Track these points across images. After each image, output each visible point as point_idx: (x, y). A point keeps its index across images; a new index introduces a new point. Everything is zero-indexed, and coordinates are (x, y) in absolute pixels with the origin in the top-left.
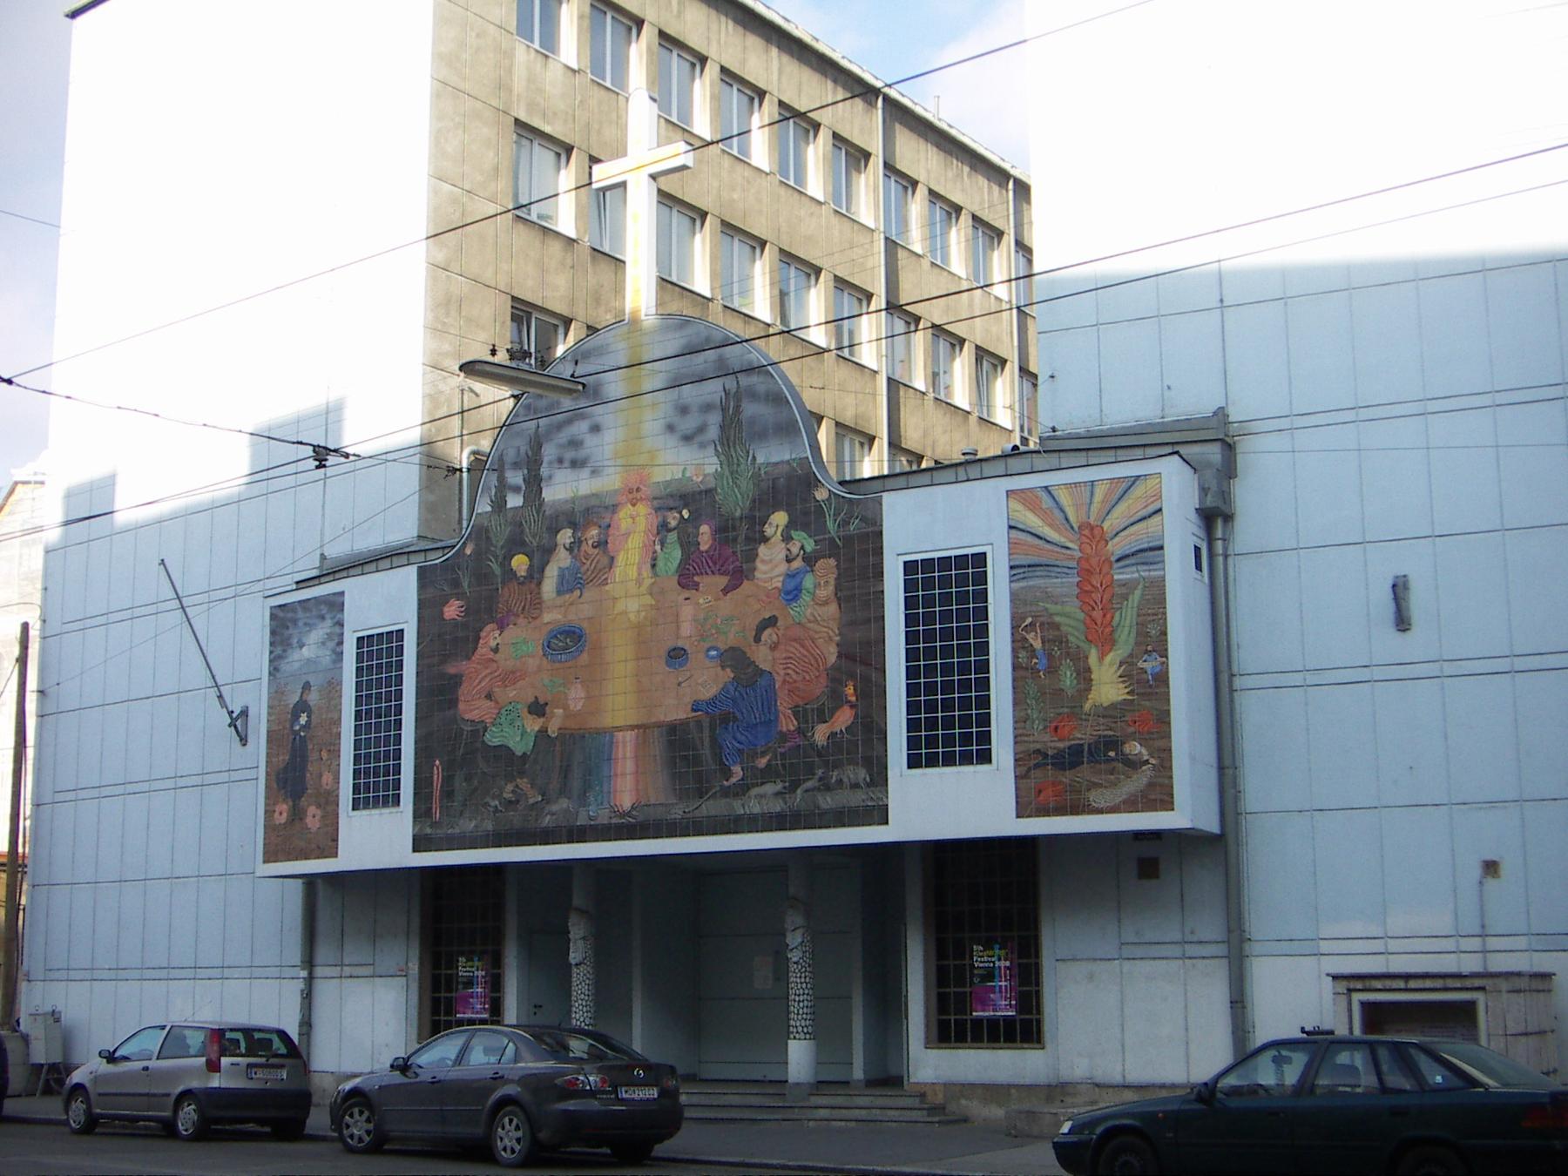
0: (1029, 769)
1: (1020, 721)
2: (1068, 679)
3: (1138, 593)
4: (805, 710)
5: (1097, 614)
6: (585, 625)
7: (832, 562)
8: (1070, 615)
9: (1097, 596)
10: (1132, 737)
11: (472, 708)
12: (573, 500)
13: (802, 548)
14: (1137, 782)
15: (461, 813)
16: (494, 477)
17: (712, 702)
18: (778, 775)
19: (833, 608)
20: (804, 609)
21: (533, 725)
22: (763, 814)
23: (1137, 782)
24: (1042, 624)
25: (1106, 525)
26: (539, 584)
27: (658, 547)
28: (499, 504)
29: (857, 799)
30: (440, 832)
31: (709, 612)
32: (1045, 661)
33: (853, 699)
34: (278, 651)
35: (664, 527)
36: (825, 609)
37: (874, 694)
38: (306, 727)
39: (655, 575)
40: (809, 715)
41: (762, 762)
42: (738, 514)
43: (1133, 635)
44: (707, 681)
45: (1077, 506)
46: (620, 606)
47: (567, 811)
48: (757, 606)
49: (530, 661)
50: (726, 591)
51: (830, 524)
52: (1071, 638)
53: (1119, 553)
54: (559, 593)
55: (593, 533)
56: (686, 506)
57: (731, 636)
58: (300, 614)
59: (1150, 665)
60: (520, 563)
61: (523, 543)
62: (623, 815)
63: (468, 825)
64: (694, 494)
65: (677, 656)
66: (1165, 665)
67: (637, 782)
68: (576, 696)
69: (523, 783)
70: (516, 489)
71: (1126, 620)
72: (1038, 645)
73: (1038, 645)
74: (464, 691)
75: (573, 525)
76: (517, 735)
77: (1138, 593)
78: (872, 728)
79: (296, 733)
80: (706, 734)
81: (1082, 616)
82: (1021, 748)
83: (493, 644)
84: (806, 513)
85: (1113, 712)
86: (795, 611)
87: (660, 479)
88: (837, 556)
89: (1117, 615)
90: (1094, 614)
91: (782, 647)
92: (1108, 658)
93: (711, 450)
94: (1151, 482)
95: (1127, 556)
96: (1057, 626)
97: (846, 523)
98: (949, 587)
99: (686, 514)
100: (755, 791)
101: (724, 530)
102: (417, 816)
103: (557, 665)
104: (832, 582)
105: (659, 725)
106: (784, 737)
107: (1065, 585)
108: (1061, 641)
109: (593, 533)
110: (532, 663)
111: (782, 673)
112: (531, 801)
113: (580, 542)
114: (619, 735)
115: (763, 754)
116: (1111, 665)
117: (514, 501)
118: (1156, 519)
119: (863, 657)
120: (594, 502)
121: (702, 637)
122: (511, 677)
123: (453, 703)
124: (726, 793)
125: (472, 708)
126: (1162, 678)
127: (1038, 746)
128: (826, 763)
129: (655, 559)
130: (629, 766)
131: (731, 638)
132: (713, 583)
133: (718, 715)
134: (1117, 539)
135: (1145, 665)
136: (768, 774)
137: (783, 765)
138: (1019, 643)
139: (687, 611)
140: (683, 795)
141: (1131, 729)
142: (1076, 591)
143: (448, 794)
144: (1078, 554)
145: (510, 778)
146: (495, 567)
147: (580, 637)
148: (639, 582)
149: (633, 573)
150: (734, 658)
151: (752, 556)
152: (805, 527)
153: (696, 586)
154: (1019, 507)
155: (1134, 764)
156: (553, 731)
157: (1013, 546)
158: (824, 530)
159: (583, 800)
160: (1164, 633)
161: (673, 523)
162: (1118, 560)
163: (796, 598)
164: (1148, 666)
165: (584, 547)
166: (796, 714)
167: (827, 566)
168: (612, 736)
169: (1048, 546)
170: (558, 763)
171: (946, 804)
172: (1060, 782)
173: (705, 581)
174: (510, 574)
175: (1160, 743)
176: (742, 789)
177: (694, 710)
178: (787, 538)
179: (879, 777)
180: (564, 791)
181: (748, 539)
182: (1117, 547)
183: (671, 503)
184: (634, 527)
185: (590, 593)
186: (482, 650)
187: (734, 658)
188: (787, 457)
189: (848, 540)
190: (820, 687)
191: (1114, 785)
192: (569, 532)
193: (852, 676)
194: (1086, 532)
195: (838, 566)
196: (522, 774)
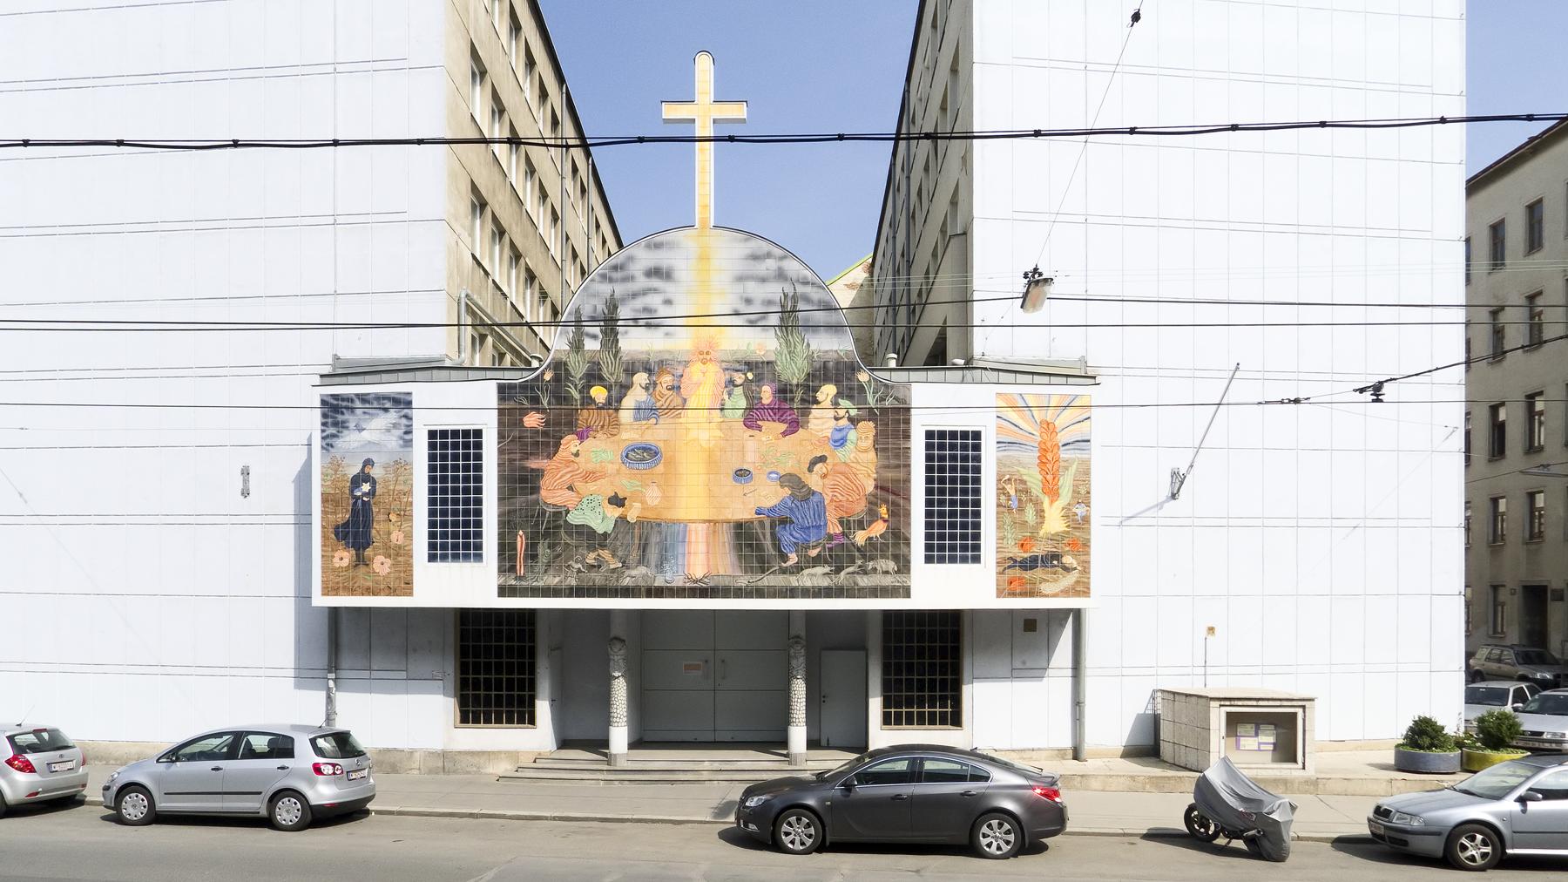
2: (1030, 515)
5: (1049, 477)
6: (661, 445)
7: (871, 424)
8: (1034, 478)
9: (1049, 466)
11: (552, 494)
14: (1071, 579)
17: (771, 510)
18: (826, 562)
19: (872, 454)
20: (846, 454)
21: (614, 513)
23: (1071, 579)
29: (888, 581)
31: (773, 449)
34: (332, 430)
37: (900, 513)
38: (372, 493)
41: (814, 553)
42: (795, 382)
44: (769, 495)
46: (693, 434)
47: (644, 576)
50: (785, 434)
56: (750, 370)
58: (358, 404)
59: (1080, 511)
60: (599, 394)
61: (601, 379)
63: (552, 580)
65: (742, 474)
68: (653, 496)
69: (606, 554)
70: (594, 337)
72: (1012, 493)
73: (1012, 493)
74: (545, 483)
75: (649, 371)
76: (601, 519)
78: (898, 537)
79: (357, 498)
80: (768, 531)
83: (574, 450)
84: (851, 389)
85: (1053, 538)
88: (875, 421)
96: (1024, 482)
99: (750, 376)
100: (806, 572)
101: (783, 391)
106: (831, 537)
107: (1031, 457)
108: (1027, 491)
109: (667, 380)
110: (611, 468)
113: (655, 384)
115: (814, 547)
117: (591, 345)
119: (892, 492)
122: (590, 476)
123: (535, 490)
124: (784, 571)
125: (552, 494)
128: (864, 557)
130: (702, 548)
131: (789, 466)
133: (780, 520)
136: (817, 561)
138: (1001, 491)
143: (532, 556)
145: (591, 548)
146: (576, 395)
150: (791, 481)
151: (805, 412)
152: (850, 397)
153: (759, 428)
155: (1067, 569)
156: (632, 518)
157: (999, 427)
159: (660, 567)
161: (739, 381)
165: (659, 388)
166: (841, 523)
167: (868, 428)
171: (936, 587)
174: (588, 401)
176: (798, 569)
178: (836, 405)
179: (904, 566)
180: (642, 561)
181: (803, 400)
182: (1062, 438)
183: (737, 366)
184: (704, 384)
186: (562, 453)
187: (791, 481)
189: (884, 410)
190: (860, 507)
192: (645, 375)
193: (886, 502)
196: (603, 546)
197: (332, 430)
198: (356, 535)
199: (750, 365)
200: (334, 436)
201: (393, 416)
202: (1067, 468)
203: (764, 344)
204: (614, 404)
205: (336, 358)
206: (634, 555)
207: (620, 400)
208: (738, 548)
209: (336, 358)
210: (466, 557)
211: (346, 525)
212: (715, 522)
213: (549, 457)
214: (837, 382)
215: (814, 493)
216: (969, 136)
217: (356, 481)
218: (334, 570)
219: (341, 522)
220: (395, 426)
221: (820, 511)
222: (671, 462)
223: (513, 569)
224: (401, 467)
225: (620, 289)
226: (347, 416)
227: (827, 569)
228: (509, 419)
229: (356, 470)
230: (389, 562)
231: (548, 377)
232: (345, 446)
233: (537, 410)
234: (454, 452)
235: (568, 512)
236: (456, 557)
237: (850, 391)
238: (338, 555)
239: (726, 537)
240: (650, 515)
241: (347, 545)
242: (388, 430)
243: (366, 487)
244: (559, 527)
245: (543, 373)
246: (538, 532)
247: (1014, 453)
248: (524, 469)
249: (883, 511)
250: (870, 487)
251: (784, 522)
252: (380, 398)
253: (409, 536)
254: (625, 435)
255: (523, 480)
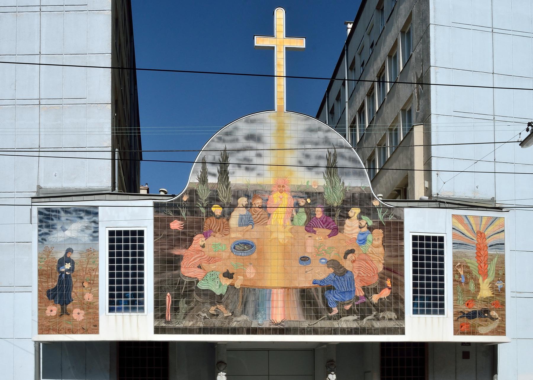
0: (458, 318)
1: (455, 300)
2: (472, 287)
3: (496, 259)
4: (368, 288)
5: (482, 265)
6: (255, 241)
9: (482, 258)
10: (493, 309)
11: (188, 270)
12: (247, 185)
13: (367, 223)
14: (494, 325)
15: (184, 318)
16: (200, 167)
18: (355, 313)
19: (381, 249)
20: (367, 248)
21: (227, 282)
22: (347, 328)
23: (494, 325)
24: (463, 266)
25: (486, 233)
26: (228, 220)
27: (295, 214)
28: (203, 180)
29: (391, 324)
30: (171, 326)
31: (320, 242)
32: (464, 279)
33: (390, 286)
35: (297, 206)
36: (377, 249)
37: (398, 284)
38: (72, 270)
39: (293, 224)
40: (368, 291)
41: (348, 307)
42: (335, 205)
43: (494, 273)
44: (321, 272)
45: (476, 224)
46: (274, 235)
48: (345, 244)
49: (224, 254)
50: (330, 236)
51: (380, 216)
52: (473, 272)
53: (490, 244)
54: (240, 225)
55: (258, 202)
56: (309, 197)
57: (333, 254)
58: (62, 214)
59: (499, 285)
60: (217, 210)
61: (218, 200)
62: (277, 324)
63: (188, 324)
64: (313, 193)
65: (304, 259)
66: (504, 285)
67: (284, 311)
68: (251, 272)
69: (221, 307)
70: (214, 175)
71: (492, 268)
72: (462, 273)
73: (462, 273)
74: (183, 264)
75: (248, 196)
76: (219, 286)
77: (496, 259)
78: (397, 299)
79: (62, 273)
81: (477, 265)
82: (456, 310)
83: (201, 243)
85: (486, 300)
86: (363, 248)
87: (296, 184)
88: (383, 229)
89: (489, 266)
90: (482, 264)
91: (356, 262)
92: (486, 281)
93: (322, 176)
94: (501, 220)
95: (492, 245)
96: (468, 267)
97: (387, 216)
98: (429, 248)
101: (329, 210)
102: (156, 317)
103: (239, 257)
104: (381, 239)
105: (296, 288)
106: (357, 298)
107: (472, 252)
108: (470, 273)
109: (258, 202)
110: (225, 255)
111: (357, 272)
112: (225, 315)
114: (275, 291)
115: (348, 304)
116: (487, 283)
117: (212, 180)
118: (502, 234)
119: (393, 271)
120: (259, 188)
121: (318, 254)
122: (211, 260)
123: (178, 268)
124: (330, 318)
125: (188, 270)
126: (503, 290)
127: (462, 310)
128: (377, 310)
129: (293, 218)
130: (280, 304)
131: (332, 256)
132: (322, 232)
134: (489, 239)
135: (498, 285)
136: (350, 312)
137: (358, 309)
139: (310, 242)
140: (308, 317)
141: (493, 307)
142: (476, 255)
144: (476, 242)
145: (213, 304)
146: (203, 210)
147: (252, 246)
148: (284, 226)
149: (281, 222)
150: (334, 264)
151: (342, 224)
152: (368, 215)
153: (315, 232)
154: (456, 221)
155: (493, 319)
156: (238, 285)
157: (454, 235)
158: (377, 217)
159: (255, 315)
160: (504, 274)
162: (490, 246)
163: (364, 243)
164: (499, 285)
166: (364, 289)
167: (379, 233)
168: (271, 291)
169: (466, 237)
170: (240, 300)
172: (469, 324)
173: (319, 230)
174: (210, 214)
175: (501, 312)
176: (338, 317)
177: (313, 283)
178: (360, 219)
179: (401, 316)
180: (244, 312)
182: (490, 241)
183: (301, 195)
184: (282, 200)
185: (257, 228)
187: (334, 264)
188: (359, 185)
189: (388, 223)
190: (375, 281)
191: (487, 325)
193: (390, 277)
194: (479, 234)
195: (383, 233)
196: (220, 303)
197: (45, 230)
198: (61, 296)
199: (309, 194)
200: (46, 234)
201: (86, 220)
202: (492, 260)
203: (317, 181)
204: (227, 215)
205: (39, 187)
206: (239, 308)
207: (230, 214)
208: (303, 304)
209: (39, 187)
210: (134, 309)
211: (55, 289)
212: (288, 288)
213: (186, 248)
214: (361, 206)
215: (347, 271)
216: (327, 167)
217: (61, 262)
218: (47, 318)
219: (51, 288)
220: (87, 228)
221: (351, 282)
222: (261, 253)
223: (163, 316)
224: (92, 254)
225: (229, 146)
226: (55, 221)
227: (355, 317)
228: (160, 225)
229: (61, 255)
230: (83, 312)
231: (185, 198)
232: (53, 240)
233: (179, 219)
234: (126, 244)
235: (198, 281)
236: (429, 312)
237: (368, 211)
238: (49, 308)
239: (295, 297)
240: (248, 284)
241: (55, 301)
242: (82, 231)
243: (68, 266)
244: (192, 291)
245: (182, 196)
246: (178, 295)
247: (462, 250)
248: (171, 255)
249: (388, 282)
250: (380, 268)
251: (330, 288)
252: (78, 210)
253: (96, 296)
254: (233, 235)
255: (170, 262)
